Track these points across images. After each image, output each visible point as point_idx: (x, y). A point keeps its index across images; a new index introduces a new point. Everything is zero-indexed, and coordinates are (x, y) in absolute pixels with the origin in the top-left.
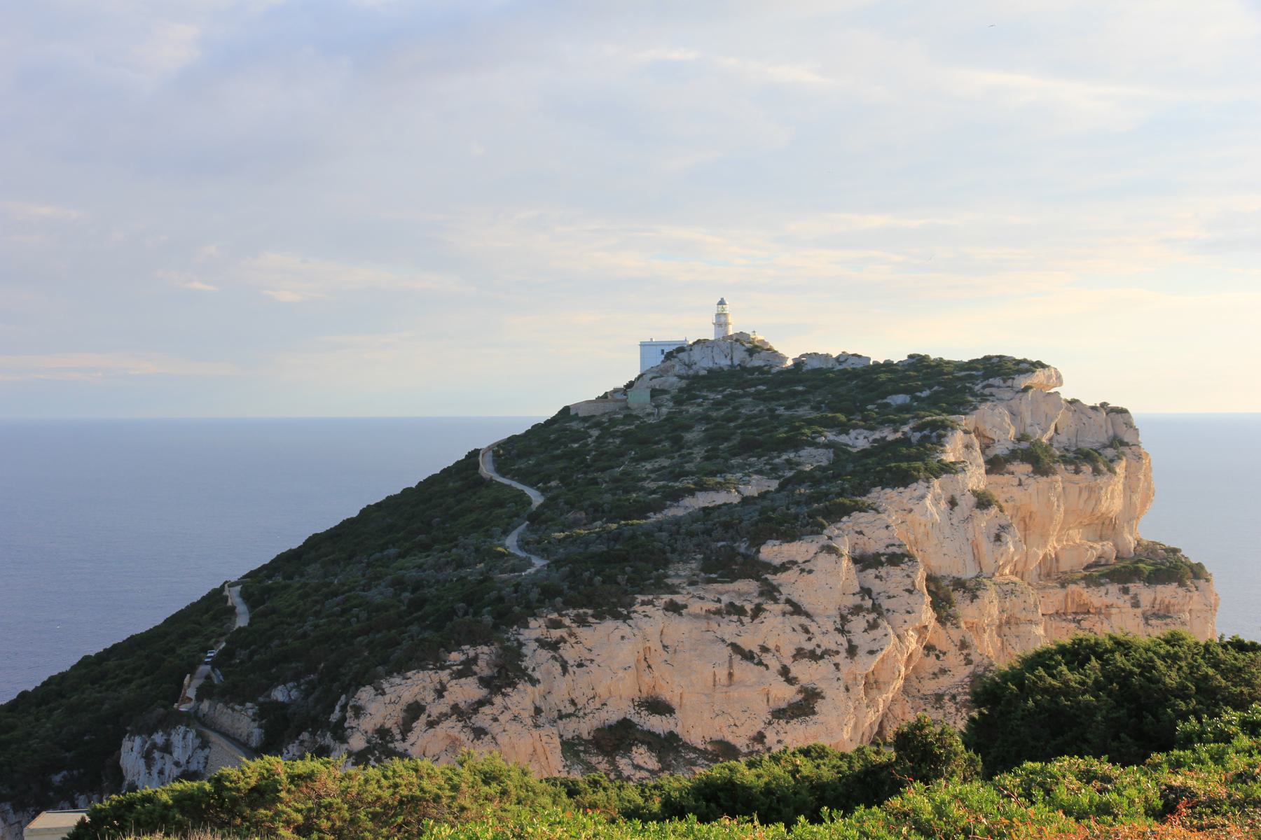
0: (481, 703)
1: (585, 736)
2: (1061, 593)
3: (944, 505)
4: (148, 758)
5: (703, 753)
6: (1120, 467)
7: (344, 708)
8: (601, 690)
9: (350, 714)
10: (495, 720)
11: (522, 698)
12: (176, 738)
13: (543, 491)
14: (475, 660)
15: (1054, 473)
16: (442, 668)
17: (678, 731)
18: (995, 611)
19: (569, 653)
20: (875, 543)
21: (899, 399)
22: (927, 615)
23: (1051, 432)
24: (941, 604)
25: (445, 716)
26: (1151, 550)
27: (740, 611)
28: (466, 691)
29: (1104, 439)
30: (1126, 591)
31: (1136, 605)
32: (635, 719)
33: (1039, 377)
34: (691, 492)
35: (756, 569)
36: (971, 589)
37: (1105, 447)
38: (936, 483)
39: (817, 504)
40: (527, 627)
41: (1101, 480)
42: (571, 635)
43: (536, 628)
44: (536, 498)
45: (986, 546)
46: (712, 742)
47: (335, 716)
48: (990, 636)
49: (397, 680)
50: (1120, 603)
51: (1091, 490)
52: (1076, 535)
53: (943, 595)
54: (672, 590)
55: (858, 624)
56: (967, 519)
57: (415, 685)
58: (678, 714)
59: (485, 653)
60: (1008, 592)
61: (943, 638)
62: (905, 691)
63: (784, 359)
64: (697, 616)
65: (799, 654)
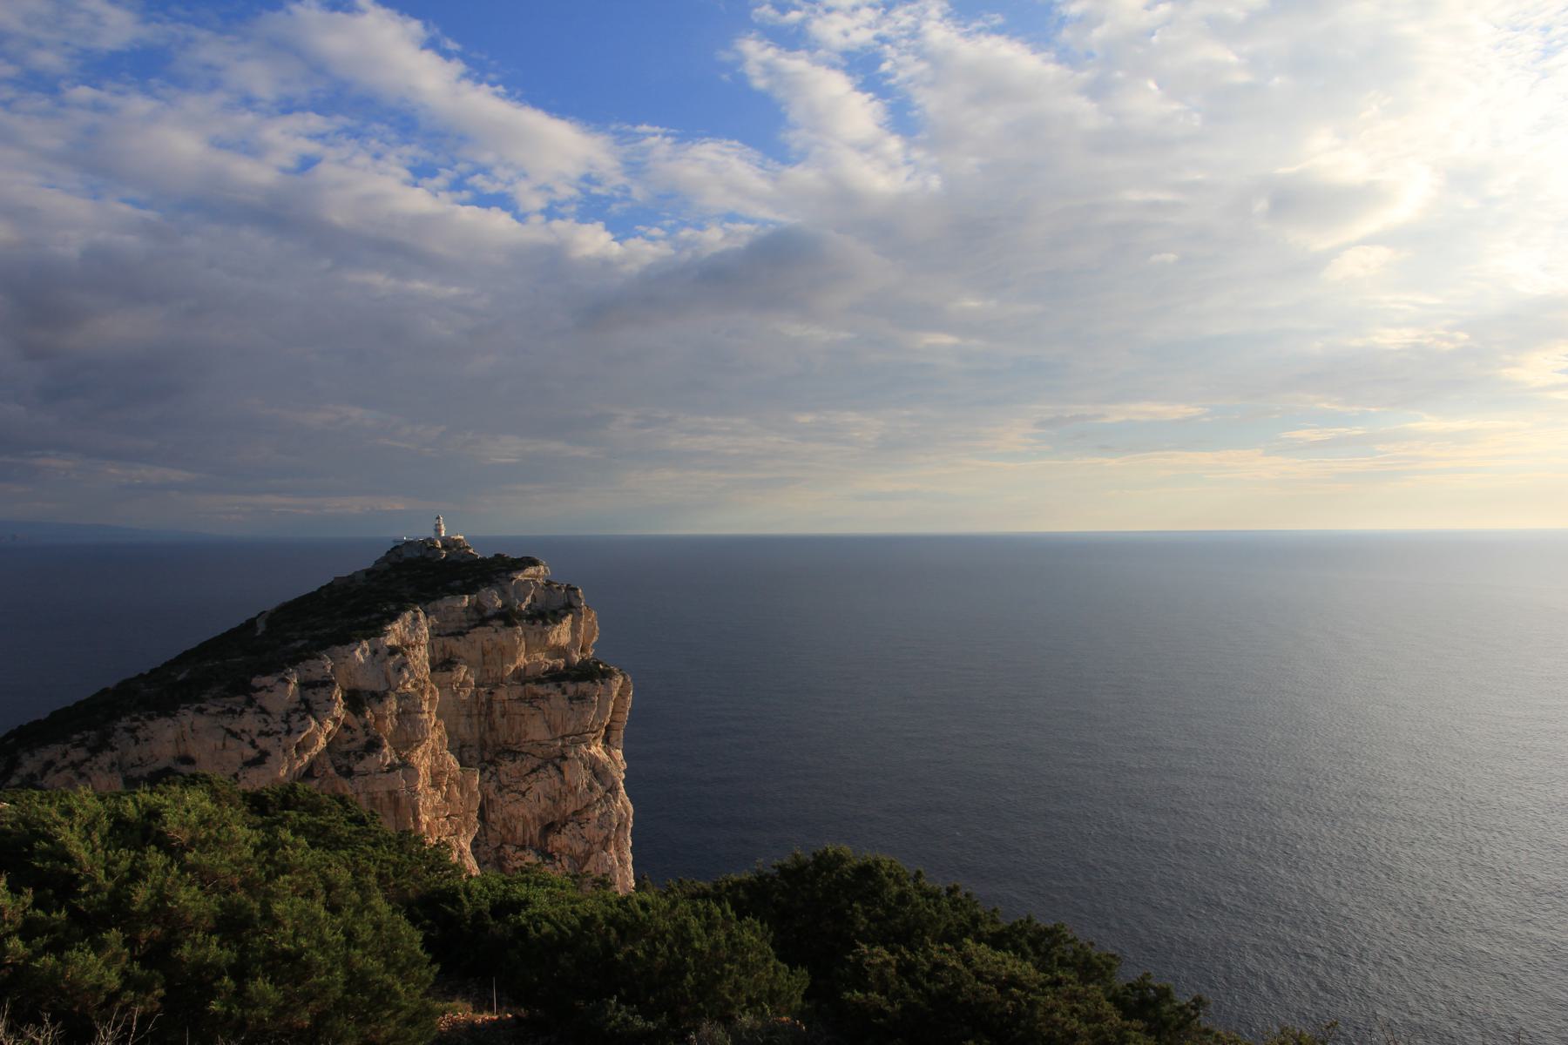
2: (521, 689)
11: (106, 758)
18: (394, 707)
19: (141, 734)
20: (316, 674)
23: (528, 599)
25: (65, 767)
28: (79, 754)
31: (564, 693)
36: (380, 697)
41: (547, 628)
43: (125, 722)
51: (542, 634)
53: (355, 701)
54: (203, 701)
55: (295, 717)
57: (46, 754)
61: (355, 722)
65: (261, 733)
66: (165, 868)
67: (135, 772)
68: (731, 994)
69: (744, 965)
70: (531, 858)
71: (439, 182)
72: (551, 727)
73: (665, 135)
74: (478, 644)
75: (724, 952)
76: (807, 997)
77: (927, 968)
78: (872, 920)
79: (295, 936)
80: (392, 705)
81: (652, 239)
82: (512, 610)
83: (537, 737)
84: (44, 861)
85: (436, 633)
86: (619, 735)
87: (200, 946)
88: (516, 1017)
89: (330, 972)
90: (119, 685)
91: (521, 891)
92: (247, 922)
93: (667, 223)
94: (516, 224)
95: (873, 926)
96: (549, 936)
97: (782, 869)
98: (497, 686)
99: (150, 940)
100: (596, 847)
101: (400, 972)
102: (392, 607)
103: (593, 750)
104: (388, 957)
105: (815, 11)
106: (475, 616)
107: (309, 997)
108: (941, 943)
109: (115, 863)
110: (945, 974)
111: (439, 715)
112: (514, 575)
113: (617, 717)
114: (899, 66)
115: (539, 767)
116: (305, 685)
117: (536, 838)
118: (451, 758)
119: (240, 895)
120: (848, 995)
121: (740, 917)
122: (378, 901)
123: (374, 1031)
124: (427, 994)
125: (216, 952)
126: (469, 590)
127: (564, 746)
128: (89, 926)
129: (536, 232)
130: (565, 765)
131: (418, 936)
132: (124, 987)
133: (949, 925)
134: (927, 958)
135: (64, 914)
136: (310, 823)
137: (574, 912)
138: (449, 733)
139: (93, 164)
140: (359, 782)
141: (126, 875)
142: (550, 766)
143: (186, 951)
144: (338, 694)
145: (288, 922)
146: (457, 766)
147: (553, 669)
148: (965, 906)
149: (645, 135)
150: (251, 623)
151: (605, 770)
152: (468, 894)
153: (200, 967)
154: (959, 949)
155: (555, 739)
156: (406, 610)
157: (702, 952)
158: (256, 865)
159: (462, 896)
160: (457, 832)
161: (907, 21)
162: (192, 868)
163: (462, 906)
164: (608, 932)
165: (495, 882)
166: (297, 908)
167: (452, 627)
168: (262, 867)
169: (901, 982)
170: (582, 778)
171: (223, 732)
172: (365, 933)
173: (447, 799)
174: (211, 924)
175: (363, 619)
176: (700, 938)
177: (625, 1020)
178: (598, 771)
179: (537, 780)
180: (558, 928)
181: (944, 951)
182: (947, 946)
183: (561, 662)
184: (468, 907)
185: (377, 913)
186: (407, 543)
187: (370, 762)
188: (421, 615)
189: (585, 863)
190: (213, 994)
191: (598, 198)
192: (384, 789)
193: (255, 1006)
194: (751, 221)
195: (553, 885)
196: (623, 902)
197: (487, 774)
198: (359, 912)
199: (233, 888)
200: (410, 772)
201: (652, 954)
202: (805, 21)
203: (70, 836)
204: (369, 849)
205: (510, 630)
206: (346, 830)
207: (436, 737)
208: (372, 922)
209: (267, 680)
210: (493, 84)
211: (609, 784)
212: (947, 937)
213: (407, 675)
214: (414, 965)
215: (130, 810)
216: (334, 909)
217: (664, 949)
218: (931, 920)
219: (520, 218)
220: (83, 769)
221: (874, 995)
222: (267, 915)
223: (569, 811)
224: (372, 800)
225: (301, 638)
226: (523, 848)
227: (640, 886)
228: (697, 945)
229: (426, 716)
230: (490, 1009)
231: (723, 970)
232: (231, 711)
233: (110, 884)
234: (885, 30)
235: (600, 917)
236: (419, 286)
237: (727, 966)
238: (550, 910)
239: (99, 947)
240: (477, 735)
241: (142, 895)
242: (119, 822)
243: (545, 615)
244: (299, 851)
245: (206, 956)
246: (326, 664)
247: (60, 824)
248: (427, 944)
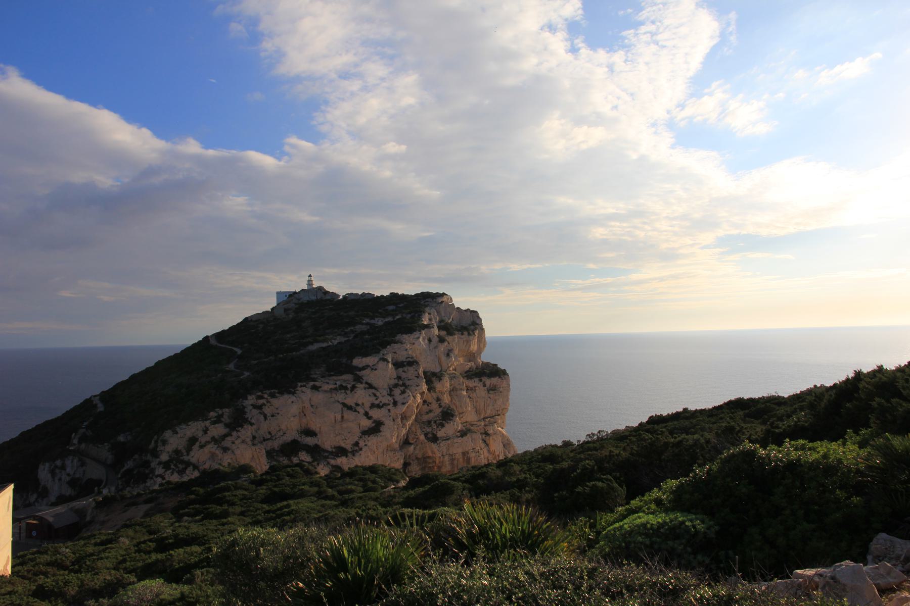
0: (226, 436)
1: (276, 448)
3: (426, 341)
4: (53, 473)
5: (331, 453)
6: (476, 333)
7: (156, 442)
8: (283, 427)
9: (160, 444)
10: (233, 443)
11: (246, 432)
12: (68, 462)
13: (241, 349)
14: (222, 416)
16: (206, 420)
17: (319, 443)
18: (448, 386)
19: (267, 410)
21: (391, 308)
22: (425, 387)
24: (429, 382)
25: (208, 443)
26: (487, 365)
27: (345, 388)
28: (218, 430)
29: (469, 322)
30: (481, 380)
31: (485, 386)
32: (299, 439)
33: (445, 299)
34: (312, 343)
35: (352, 370)
36: (439, 376)
38: (423, 332)
39: (377, 342)
40: (246, 399)
41: (471, 337)
42: (268, 402)
43: (251, 400)
44: (239, 352)
45: (443, 358)
46: (335, 447)
47: (152, 445)
49: (184, 426)
52: (461, 360)
54: (314, 380)
55: (397, 391)
56: (436, 347)
57: (193, 428)
58: (319, 436)
59: (227, 411)
60: (453, 377)
62: (416, 420)
63: (339, 296)
64: (326, 391)
72: (478, 412)
127: (485, 425)
171: (340, 406)
187: (450, 429)
192: (460, 450)
209: (369, 360)
232: (342, 388)
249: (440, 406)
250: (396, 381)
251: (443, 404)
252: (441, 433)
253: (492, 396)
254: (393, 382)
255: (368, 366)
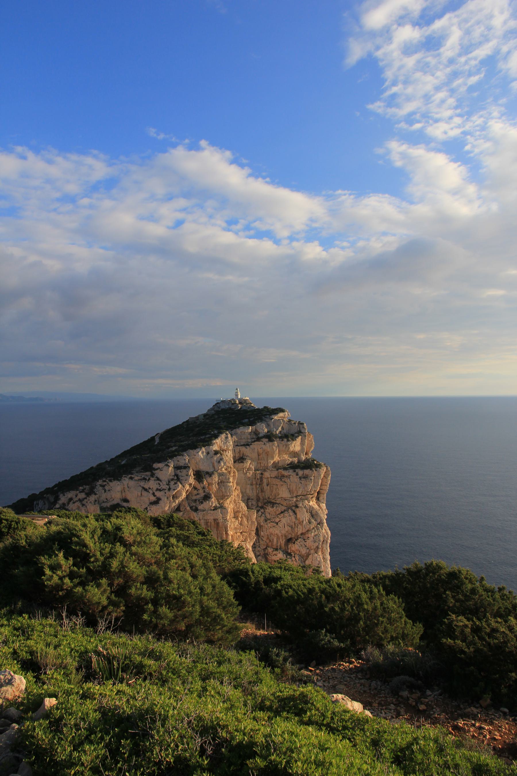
0: (86, 498)
2: (276, 472)
3: (205, 454)
8: (113, 496)
11: (93, 498)
14: (85, 489)
15: (274, 441)
18: (217, 479)
19: (107, 488)
20: (181, 463)
23: (280, 429)
25: (77, 501)
28: (82, 496)
29: (296, 431)
30: (295, 471)
31: (297, 475)
36: (210, 474)
37: (296, 433)
41: (289, 443)
42: (108, 484)
43: (100, 482)
48: (215, 485)
50: (293, 474)
53: (199, 476)
54: (132, 474)
59: (87, 487)
61: (198, 486)
64: (136, 480)
66: (124, 553)
67: (105, 505)
68: (383, 633)
69: (389, 619)
70: (280, 555)
71: (239, 227)
72: (290, 491)
73: (350, 195)
74: (256, 450)
75: (379, 612)
76: (422, 638)
77: (488, 630)
78: (457, 601)
79: (178, 588)
80: (216, 478)
81: (343, 248)
82: (272, 434)
83: (284, 496)
84: (76, 546)
85: (236, 445)
86: (324, 497)
87: (139, 589)
88: (276, 634)
89: (193, 606)
90: (98, 465)
91: (277, 573)
92: (158, 579)
93: (351, 239)
94: (275, 246)
95: (458, 604)
96: (292, 596)
97: (408, 570)
98: (265, 471)
99: (118, 585)
100: (312, 551)
101: (224, 608)
102: (216, 432)
103: (311, 503)
104: (218, 600)
105: (428, 123)
106: (254, 437)
107: (184, 617)
108: (495, 617)
109: (103, 549)
110: (498, 635)
111: (237, 484)
112: (273, 416)
113: (323, 487)
114: (476, 146)
115: (285, 511)
116: (177, 468)
117: (283, 545)
118: (243, 505)
119: (154, 568)
120: (444, 640)
121: (388, 594)
122: (214, 574)
123: (212, 635)
124: (235, 620)
125: (146, 593)
126: (252, 424)
127: (297, 501)
128: (95, 576)
129: (283, 250)
130: (297, 511)
131: (232, 592)
132: (109, 604)
133: (500, 608)
134: (488, 625)
135: (85, 570)
136: (180, 534)
137: (304, 585)
138: (242, 492)
139: (88, 233)
140: (201, 514)
141: (108, 555)
142: (290, 511)
143: (133, 591)
144: (191, 472)
145: (175, 581)
146: (245, 508)
147: (291, 463)
148: (509, 598)
149: (340, 195)
150: (153, 439)
151: (317, 514)
152: (253, 572)
153: (139, 598)
154: (506, 621)
155: (292, 497)
156: (222, 433)
157: (368, 611)
158: (161, 554)
159: (250, 573)
160: (245, 540)
161: (480, 121)
162: (135, 554)
163: (250, 578)
164: (321, 596)
165: (265, 567)
166: (179, 576)
167: (243, 442)
168: (163, 555)
169: (474, 637)
170: (304, 516)
171: (141, 488)
172: (209, 590)
173: (241, 524)
174: (143, 580)
175: (203, 437)
176: (367, 604)
177: (329, 641)
178: (313, 514)
179: (284, 517)
180: (297, 593)
181: (497, 622)
182: (499, 620)
183: (296, 460)
184: (253, 579)
185: (213, 580)
186: (223, 401)
187: (206, 505)
188: (229, 435)
189: (307, 559)
190: (144, 611)
191: (316, 229)
192: (212, 518)
193: (162, 619)
194: (394, 235)
195: (293, 571)
196: (328, 581)
197: (260, 513)
198: (205, 579)
199: (151, 564)
200: (224, 510)
201: (343, 609)
202: (423, 128)
203: (86, 536)
204: (207, 548)
205: (271, 443)
206: (197, 538)
207: (236, 494)
208: (211, 584)
209: (160, 465)
210: (264, 178)
211: (319, 521)
212: (497, 614)
213: (222, 464)
214: (230, 606)
215: (109, 527)
216: (194, 577)
217: (348, 608)
218: (489, 604)
219: (277, 242)
220: (84, 502)
221: (459, 642)
222: (166, 577)
223: (299, 533)
224: (207, 523)
225: (175, 446)
226: (276, 549)
227: (334, 574)
228: (366, 607)
229: (231, 484)
230: (263, 629)
231: (378, 620)
232: (144, 479)
233: (102, 558)
234: (468, 127)
235: (317, 589)
236: (230, 277)
237: (381, 619)
238: (292, 583)
239: (99, 586)
240: (255, 494)
241: (115, 564)
242: (105, 531)
243: (288, 436)
244: (180, 549)
245: (142, 594)
246: (185, 458)
247: (82, 531)
248: (236, 596)
249: (204, 492)
250: (173, 477)
251: (206, 491)
252: (200, 507)
253: (303, 482)
254: (172, 477)
255: (159, 468)
